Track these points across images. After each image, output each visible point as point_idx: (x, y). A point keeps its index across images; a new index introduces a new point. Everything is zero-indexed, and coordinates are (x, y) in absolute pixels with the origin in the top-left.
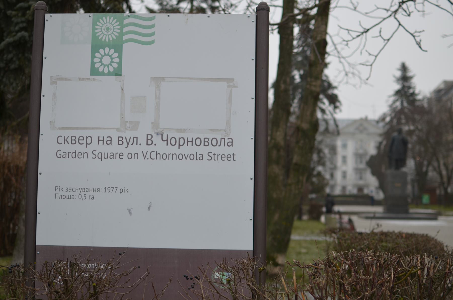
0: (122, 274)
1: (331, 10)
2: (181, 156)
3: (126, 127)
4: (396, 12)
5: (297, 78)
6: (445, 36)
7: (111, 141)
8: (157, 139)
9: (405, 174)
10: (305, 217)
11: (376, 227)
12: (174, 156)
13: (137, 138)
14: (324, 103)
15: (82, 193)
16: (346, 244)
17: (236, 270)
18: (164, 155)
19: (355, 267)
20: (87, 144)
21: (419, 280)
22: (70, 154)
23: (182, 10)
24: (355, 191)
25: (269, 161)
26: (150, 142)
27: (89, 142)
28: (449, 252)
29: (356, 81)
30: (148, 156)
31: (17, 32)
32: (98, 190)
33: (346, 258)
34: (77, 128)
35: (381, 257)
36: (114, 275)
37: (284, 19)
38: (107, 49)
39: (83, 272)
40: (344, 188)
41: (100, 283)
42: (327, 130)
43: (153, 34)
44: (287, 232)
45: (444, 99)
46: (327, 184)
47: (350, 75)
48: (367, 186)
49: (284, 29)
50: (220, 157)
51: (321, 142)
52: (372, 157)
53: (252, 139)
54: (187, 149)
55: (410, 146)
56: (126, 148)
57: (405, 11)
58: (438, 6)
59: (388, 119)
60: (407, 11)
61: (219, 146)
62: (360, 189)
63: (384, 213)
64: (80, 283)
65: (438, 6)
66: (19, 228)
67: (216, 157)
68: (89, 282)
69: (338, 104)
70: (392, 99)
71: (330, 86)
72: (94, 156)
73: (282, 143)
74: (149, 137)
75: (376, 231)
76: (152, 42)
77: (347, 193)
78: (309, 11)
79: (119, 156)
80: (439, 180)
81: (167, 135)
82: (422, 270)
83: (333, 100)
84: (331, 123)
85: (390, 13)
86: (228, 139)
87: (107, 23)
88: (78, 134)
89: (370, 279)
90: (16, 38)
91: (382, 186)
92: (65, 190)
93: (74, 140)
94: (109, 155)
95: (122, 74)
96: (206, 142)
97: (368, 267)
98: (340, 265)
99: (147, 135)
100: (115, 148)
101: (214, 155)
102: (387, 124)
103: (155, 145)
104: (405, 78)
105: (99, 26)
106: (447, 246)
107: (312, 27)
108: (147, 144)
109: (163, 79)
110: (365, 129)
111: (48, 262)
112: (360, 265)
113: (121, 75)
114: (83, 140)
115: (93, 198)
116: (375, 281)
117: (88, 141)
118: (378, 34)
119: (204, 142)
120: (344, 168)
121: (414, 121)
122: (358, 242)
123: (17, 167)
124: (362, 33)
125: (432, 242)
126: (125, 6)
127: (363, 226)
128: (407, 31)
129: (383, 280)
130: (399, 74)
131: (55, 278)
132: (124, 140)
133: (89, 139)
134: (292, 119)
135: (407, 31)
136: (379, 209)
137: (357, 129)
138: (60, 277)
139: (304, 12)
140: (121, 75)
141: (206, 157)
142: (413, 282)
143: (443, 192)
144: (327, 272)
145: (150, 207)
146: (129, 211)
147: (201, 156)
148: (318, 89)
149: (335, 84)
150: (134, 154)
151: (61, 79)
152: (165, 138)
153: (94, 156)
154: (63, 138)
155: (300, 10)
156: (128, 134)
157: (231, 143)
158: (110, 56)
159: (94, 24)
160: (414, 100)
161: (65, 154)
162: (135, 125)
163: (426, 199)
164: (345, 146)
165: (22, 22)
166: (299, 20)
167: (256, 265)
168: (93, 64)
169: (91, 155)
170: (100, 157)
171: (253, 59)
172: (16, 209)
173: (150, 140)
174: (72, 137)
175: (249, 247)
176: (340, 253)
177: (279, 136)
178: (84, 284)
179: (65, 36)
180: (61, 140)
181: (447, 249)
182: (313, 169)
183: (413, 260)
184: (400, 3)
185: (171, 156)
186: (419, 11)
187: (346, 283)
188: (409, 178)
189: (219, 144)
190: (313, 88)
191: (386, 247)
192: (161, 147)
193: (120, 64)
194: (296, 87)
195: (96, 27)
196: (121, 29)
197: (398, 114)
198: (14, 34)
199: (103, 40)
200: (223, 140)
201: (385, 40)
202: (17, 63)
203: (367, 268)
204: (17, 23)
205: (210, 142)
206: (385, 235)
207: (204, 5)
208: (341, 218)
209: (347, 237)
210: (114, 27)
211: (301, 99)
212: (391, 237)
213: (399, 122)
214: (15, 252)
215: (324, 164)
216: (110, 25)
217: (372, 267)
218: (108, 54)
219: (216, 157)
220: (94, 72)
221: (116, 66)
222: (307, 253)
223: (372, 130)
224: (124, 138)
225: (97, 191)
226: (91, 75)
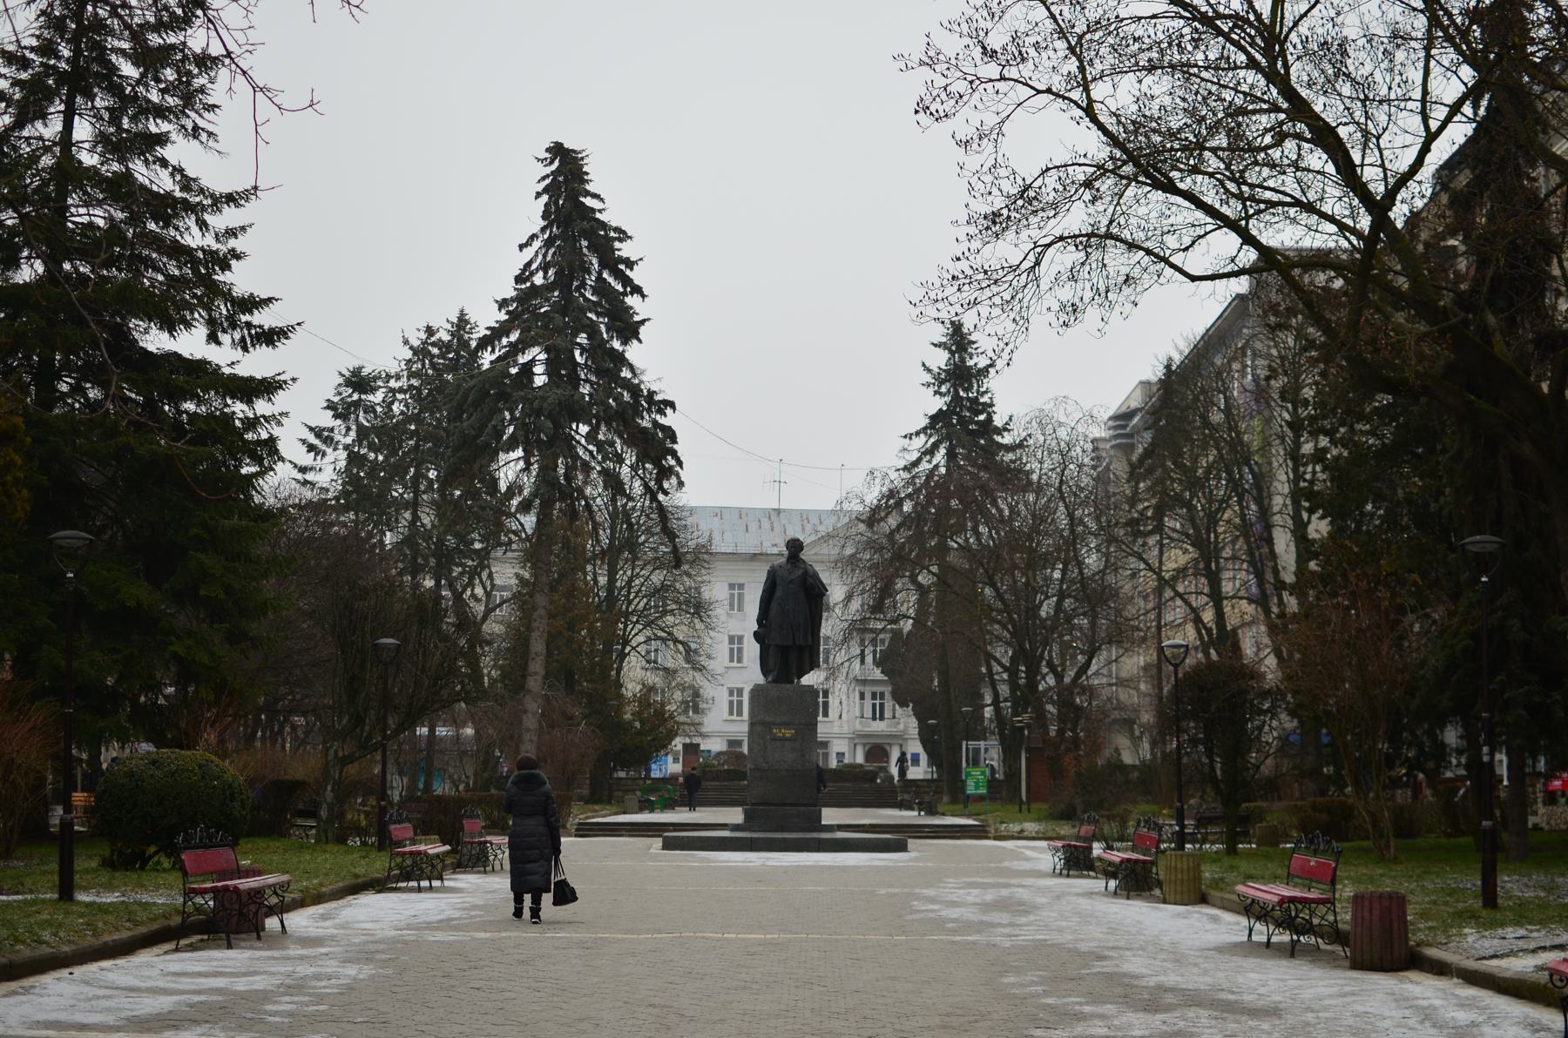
62: (877, 752)
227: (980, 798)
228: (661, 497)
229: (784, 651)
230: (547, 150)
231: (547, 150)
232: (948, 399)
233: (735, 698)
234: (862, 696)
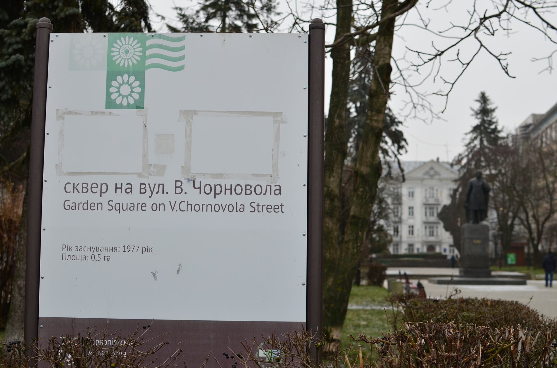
0: (148, 352)
1: (395, 29)
2: (217, 207)
3: (150, 172)
4: (476, 30)
5: (353, 113)
6: (534, 60)
7: (131, 188)
8: (187, 187)
9: (487, 228)
10: (364, 282)
11: (454, 293)
12: (209, 207)
13: (163, 185)
14: (386, 143)
15: (96, 253)
16: (419, 314)
17: (287, 346)
18: (197, 206)
19: (434, 342)
20: (101, 192)
21: (512, 357)
22: (81, 205)
23: (211, 29)
24: (425, 250)
25: (324, 214)
26: (179, 190)
27: (104, 190)
28: (545, 322)
29: (427, 114)
30: (177, 207)
31: (10, 55)
32: (116, 249)
33: (422, 330)
34: (89, 174)
35: (466, 330)
36: (138, 353)
37: (339, 40)
38: (126, 77)
39: (99, 350)
40: (411, 246)
41: (121, 363)
42: (389, 174)
43: (182, 58)
44: (344, 300)
45: (533, 136)
46: (391, 241)
47: (419, 107)
48: (440, 243)
49: (339, 52)
50: (265, 208)
51: (383, 189)
52: (445, 207)
53: (304, 185)
54: (224, 199)
55: (491, 194)
56: (150, 197)
57: (489, 30)
58: (526, 23)
59: (464, 161)
60: (490, 28)
61: (265, 194)
62: (431, 247)
63: (460, 276)
64: (96, 363)
65: (526, 23)
66: (12, 296)
67: (260, 208)
68: (106, 362)
69: (403, 143)
70: (470, 136)
71: (393, 121)
72: (111, 208)
73: (337, 191)
74: (178, 184)
75: (453, 298)
76: (182, 68)
77: (415, 252)
78: (369, 30)
79: (142, 207)
80: (527, 236)
81: (200, 181)
82: (516, 344)
83: (398, 138)
84: (395, 165)
85: (468, 32)
86: (275, 186)
87: (123, 45)
88: (90, 180)
89: (453, 357)
90: (10, 62)
91: (457, 244)
92: (74, 249)
93: (85, 188)
94: (129, 206)
95: (146, 106)
96: (248, 190)
97: (451, 341)
98: (416, 341)
99: (176, 181)
100: (136, 197)
101: (258, 205)
102: (463, 167)
103: (186, 193)
104: (485, 111)
105: (115, 48)
106: (542, 316)
107: (372, 49)
108: (176, 193)
109: (195, 112)
110: (437, 173)
111: (55, 338)
112: (439, 339)
113: (143, 108)
114: (97, 187)
115: (109, 259)
116: (460, 359)
117: (103, 188)
118: (457, 58)
119: (246, 190)
120: (411, 222)
121: (496, 164)
122: (433, 312)
123: (10, 221)
124: (436, 56)
125: (524, 311)
126: (143, 24)
127: (435, 292)
128: (490, 53)
129: (469, 357)
130: (477, 106)
131: (64, 356)
132: (147, 188)
133: (104, 187)
134: (348, 161)
135: (490, 53)
136: (455, 272)
137: (427, 173)
138: (70, 356)
139: (362, 31)
140: (143, 108)
141: (248, 208)
142: (503, 360)
143: (532, 251)
144: (400, 348)
145: (179, 270)
146: (154, 274)
147: (242, 207)
148: (381, 125)
149: (399, 118)
150: (160, 205)
151: (70, 113)
152: (197, 185)
153: (111, 208)
154: (72, 185)
155: (357, 29)
156: (153, 181)
157: (279, 191)
158: (130, 85)
159: (110, 46)
160: (497, 138)
161: (74, 204)
162: (161, 169)
163: (511, 258)
164: (411, 195)
165: (17, 43)
166: (357, 40)
167: (312, 340)
168: (108, 94)
169: (106, 207)
170: (117, 208)
171: (305, 88)
172: (9, 274)
173: (179, 187)
174: (83, 184)
175: (302, 317)
176: (415, 324)
177: (333, 183)
178: (100, 365)
179: (73, 61)
180: (70, 188)
181: (543, 320)
182: (374, 222)
183: (505, 333)
184: (481, 19)
185: (205, 207)
186: (504, 29)
187: (424, 360)
188: (491, 233)
189: (264, 192)
190: (375, 124)
191: (469, 317)
192: (192, 196)
193: (142, 94)
194: (352, 122)
195: (141, 54)
196: (144, 52)
197: (476, 155)
198: (6, 57)
199: (121, 65)
200: (268, 187)
201: (463, 64)
202: (10, 92)
203: (449, 343)
204: (11, 44)
205: (253, 189)
206: (467, 303)
207: (239, 23)
208: (408, 282)
209: (419, 305)
210: (134, 49)
211: (358, 137)
212: (474, 305)
213: (478, 165)
214: (8, 327)
215: (386, 217)
216: (130, 46)
217: (456, 342)
218: (127, 83)
219: (260, 208)
220: (110, 104)
221: (137, 96)
222: (367, 326)
223: (445, 174)
224: (147, 186)
225: (114, 250)
226: (106, 108)
227: (512, 265)
228: (399, 156)
229: (476, 212)
230: (83, 32)
231: (83, 32)
232: (480, 120)
234: (426, 228)
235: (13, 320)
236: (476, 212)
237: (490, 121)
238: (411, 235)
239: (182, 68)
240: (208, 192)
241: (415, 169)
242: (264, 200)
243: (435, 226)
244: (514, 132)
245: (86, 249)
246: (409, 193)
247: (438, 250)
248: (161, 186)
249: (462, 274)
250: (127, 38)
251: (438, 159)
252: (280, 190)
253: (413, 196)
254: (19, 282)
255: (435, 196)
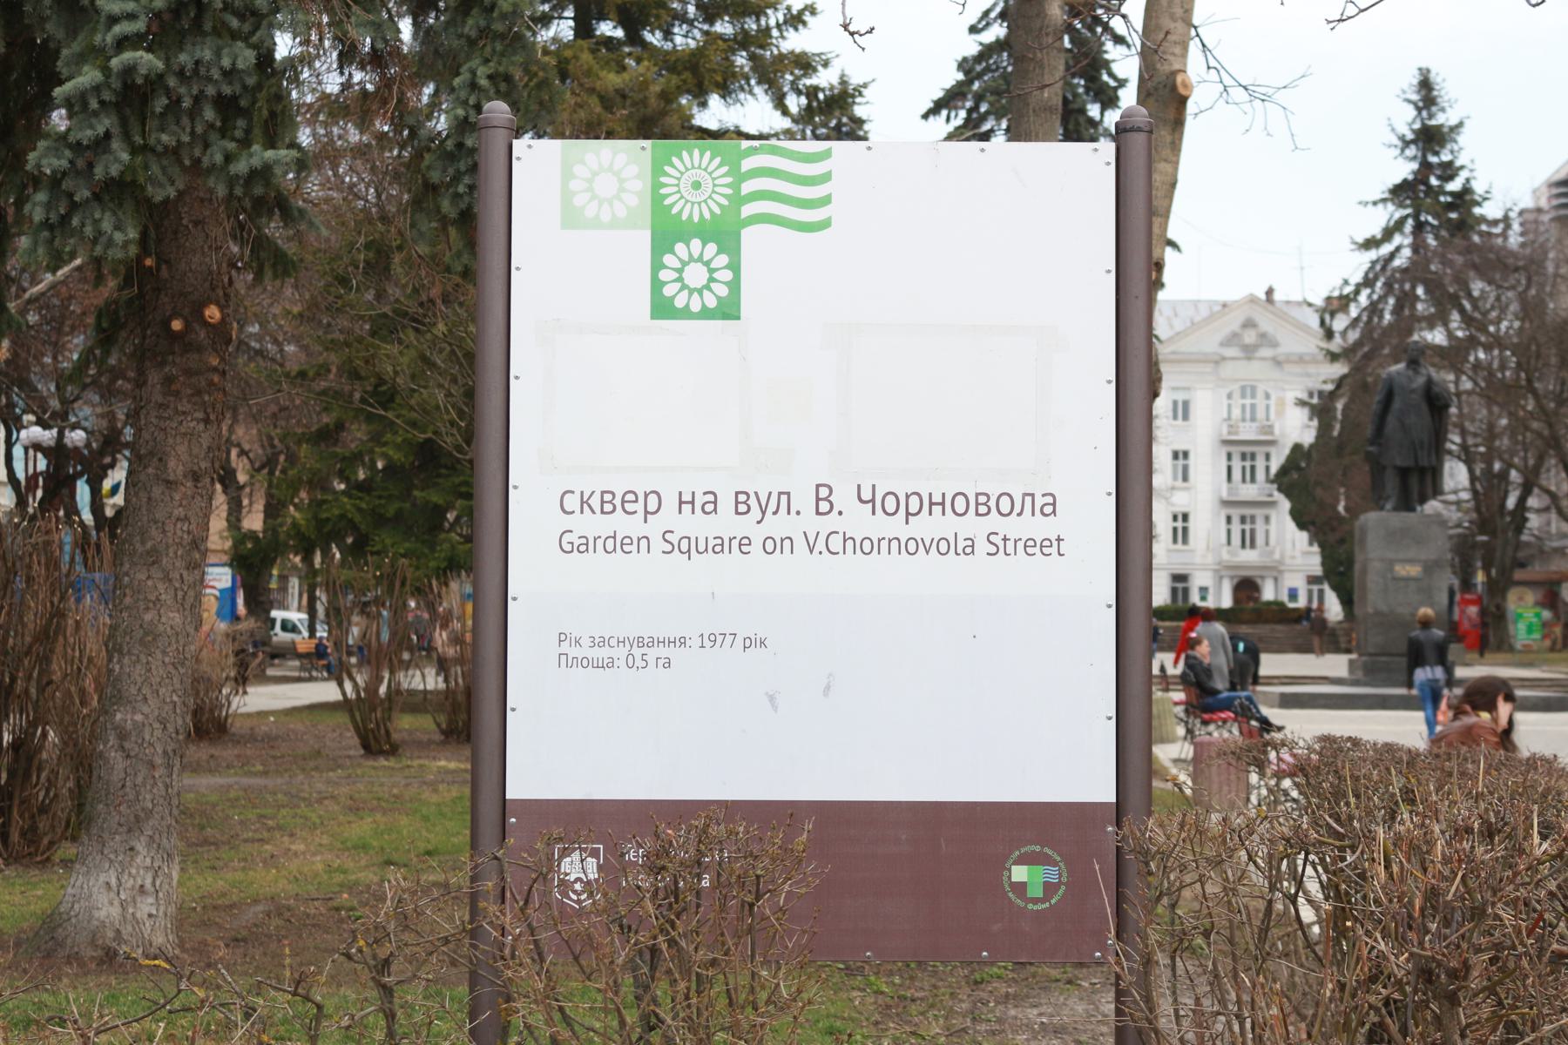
7: (715, 503)
12: (895, 544)
15: (637, 652)
18: (867, 543)
20: (646, 512)
22: (600, 542)
26: (824, 506)
27: (652, 507)
30: (821, 545)
43: (826, 200)
48: (1276, 572)
50: (1020, 545)
54: (929, 526)
61: (1019, 514)
62: (1246, 587)
67: (1010, 544)
72: (669, 548)
74: (824, 492)
76: (825, 224)
91: (1339, 570)
92: (586, 642)
93: (608, 503)
94: (711, 543)
96: (982, 505)
99: (818, 486)
100: (726, 523)
101: (1005, 539)
103: (840, 513)
108: (818, 513)
110: (1265, 339)
115: (668, 664)
117: (648, 503)
119: (977, 504)
120: (1181, 501)
130: (1405, 119)
132: (753, 502)
133: (653, 499)
136: (1336, 664)
137: (1232, 339)
141: (982, 547)
145: (828, 688)
146: (772, 698)
152: (867, 496)
153: (669, 548)
168: (657, 285)
169: (658, 545)
170: (684, 549)
180: (572, 502)
185: (884, 544)
189: (1017, 509)
192: (859, 521)
196: (736, 186)
199: (696, 219)
205: (992, 503)
219: (1010, 544)
227: (1527, 649)
229: (1404, 473)
232: (1415, 166)
233: (1179, 524)
234: (1229, 520)
235: (102, 829)
236: (1404, 473)
237: (1450, 164)
238: (1180, 546)
239: (825, 224)
240: (891, 509)
241: (1194, 326)
242: (1017, 527)
243: (1259, 513)
244: (1527, 202)
245: (613, 642)
246: (1175, 403)
247: (1268, 594)
248: (784, 498)
249: (1360, 674)
250: (696, 152)
251: (1270, 292)
252: (1054, 504)
253: (1186, 417)
254: (119, 716)
255: (1261, 414)
